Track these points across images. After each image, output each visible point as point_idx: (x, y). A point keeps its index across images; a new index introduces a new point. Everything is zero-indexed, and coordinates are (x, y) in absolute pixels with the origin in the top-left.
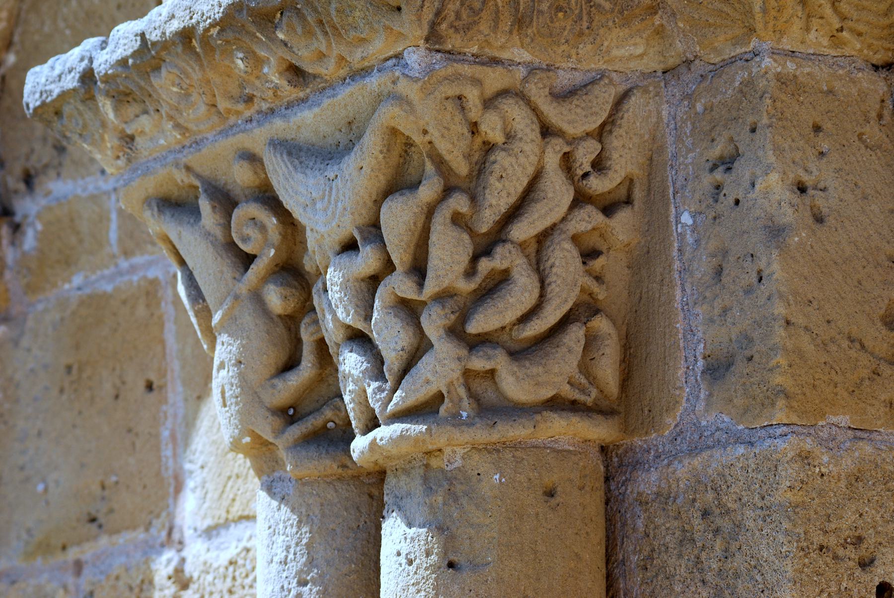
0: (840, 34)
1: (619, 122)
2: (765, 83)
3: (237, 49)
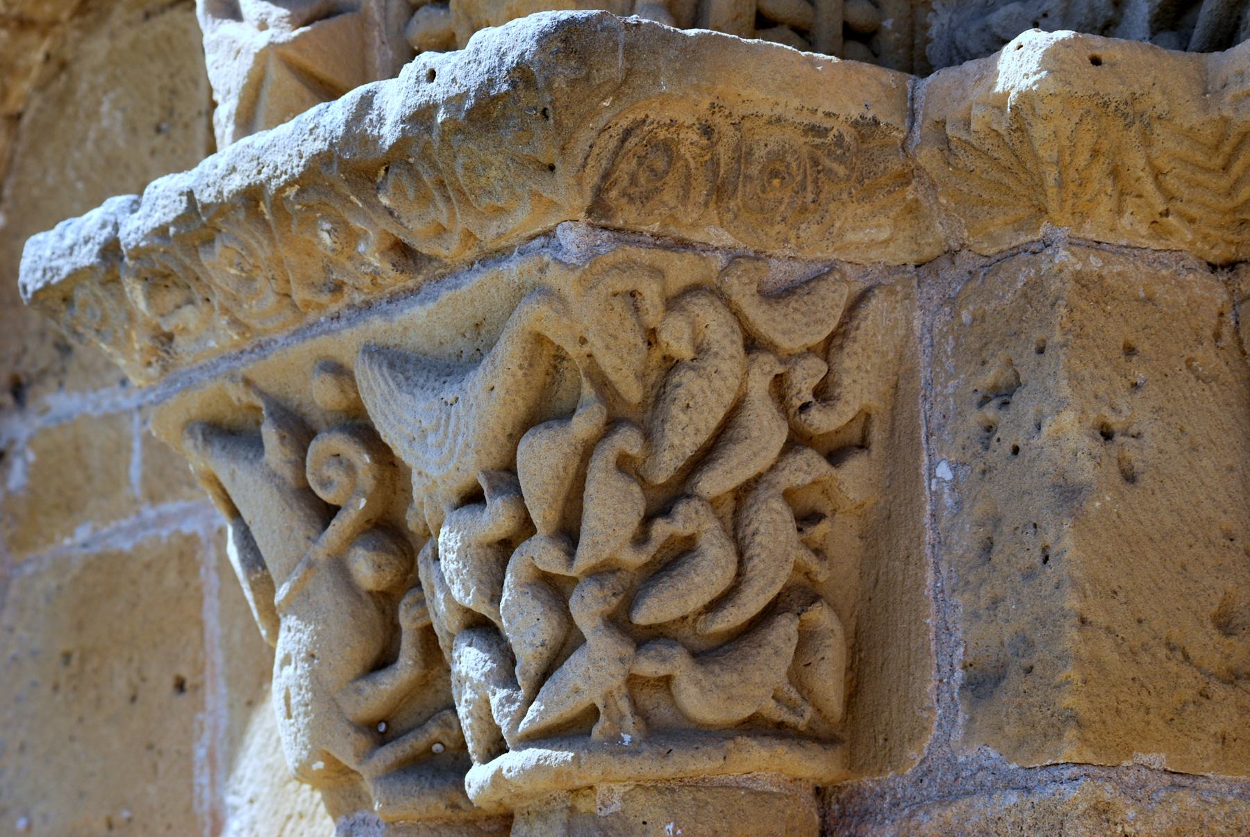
0: (1164, 219)
1: (853, 334)
2: (1059, 284)
3: (322, 217)
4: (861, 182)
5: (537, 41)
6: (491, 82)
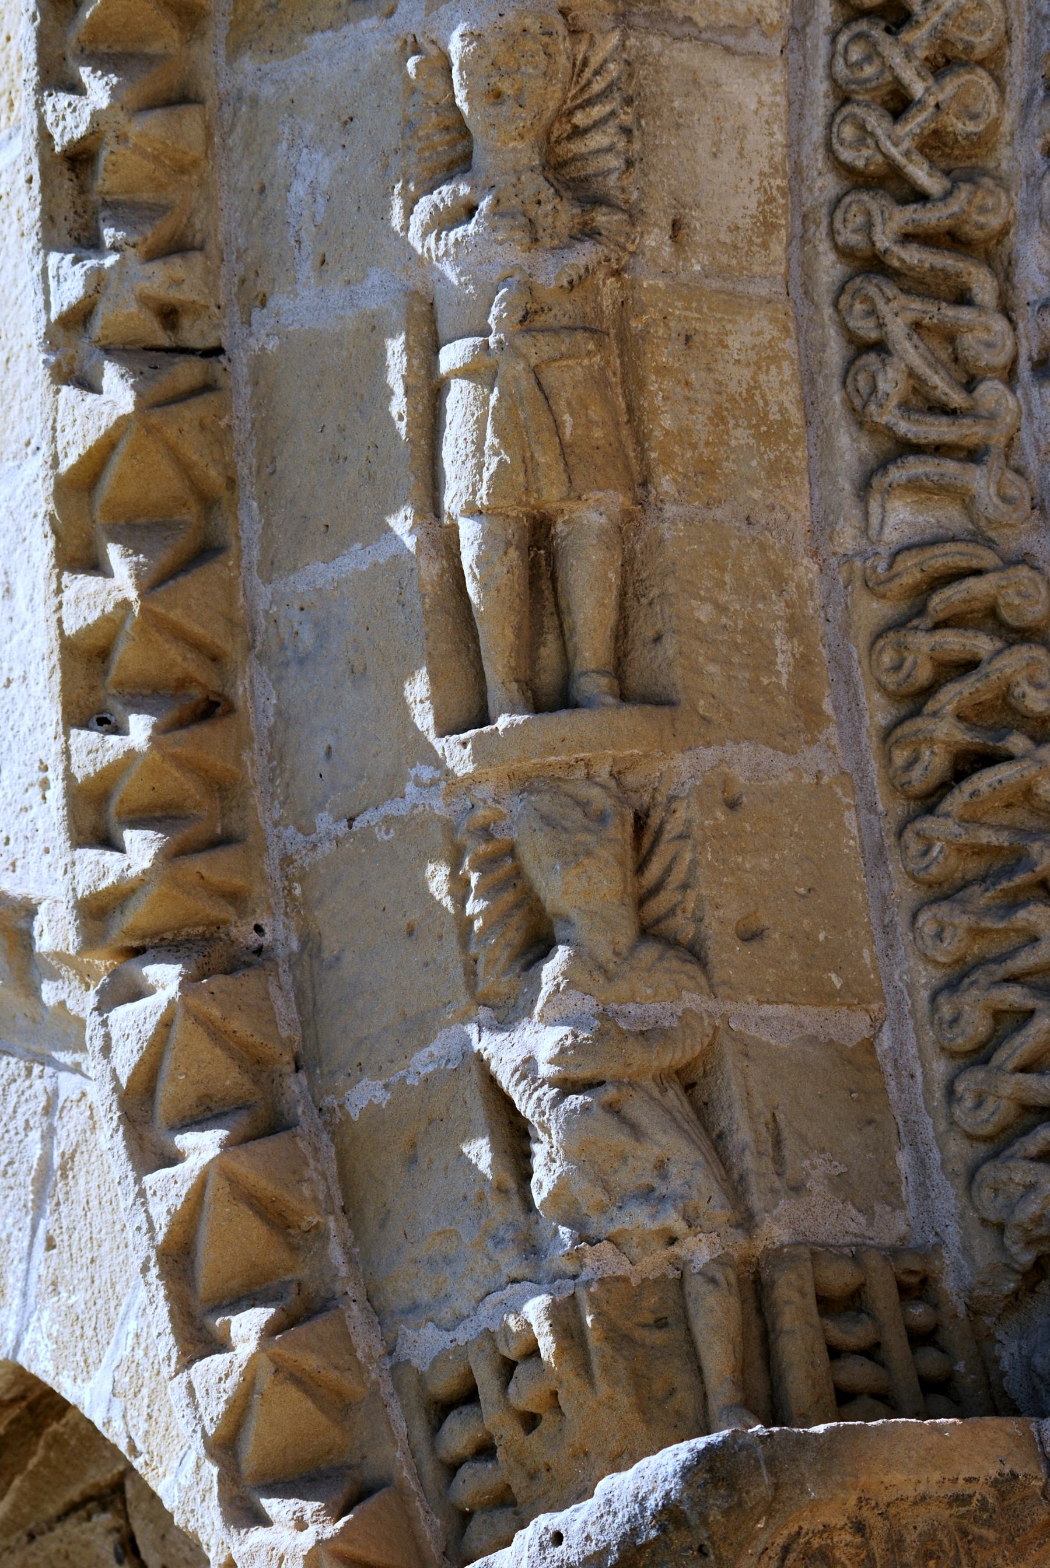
4: (1011, 1541)
5: (681, 1477)
6: (635, 1532)
